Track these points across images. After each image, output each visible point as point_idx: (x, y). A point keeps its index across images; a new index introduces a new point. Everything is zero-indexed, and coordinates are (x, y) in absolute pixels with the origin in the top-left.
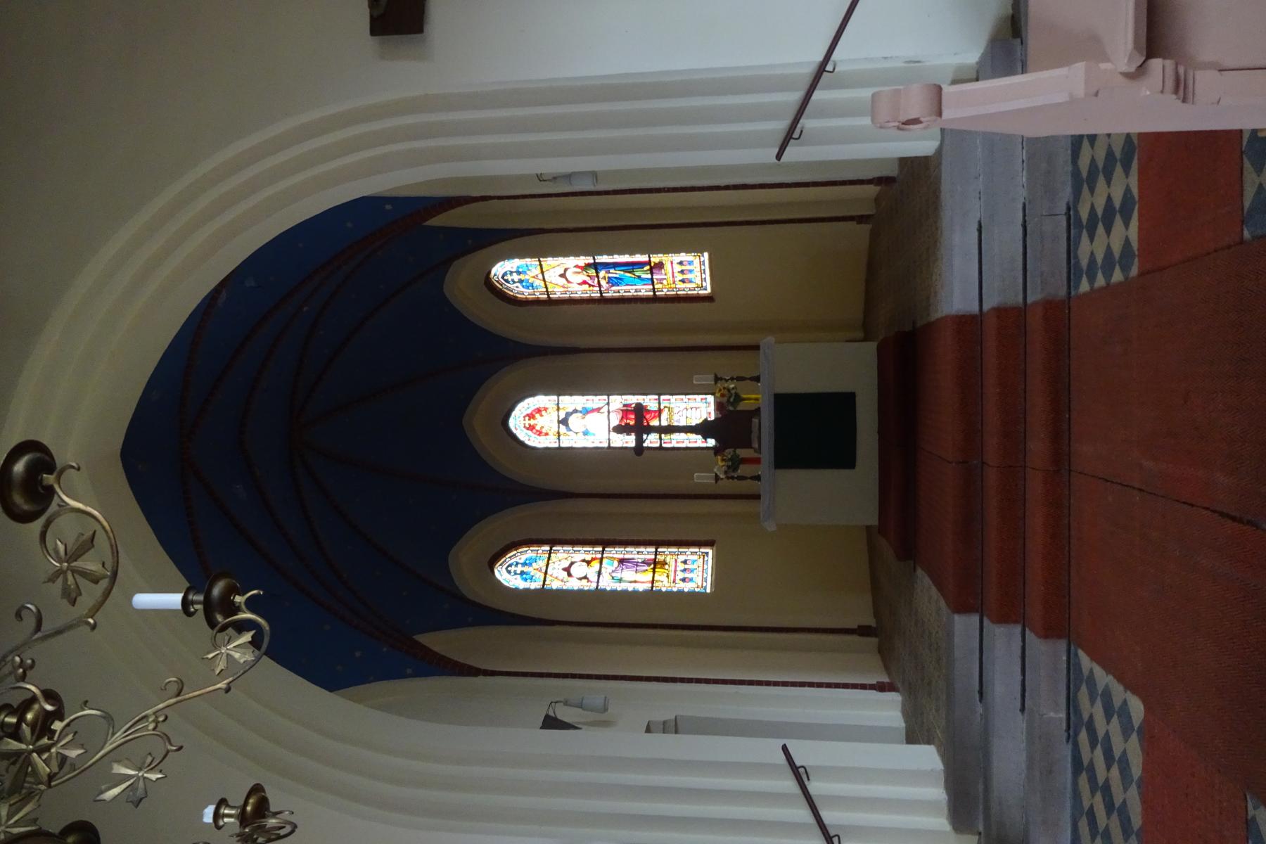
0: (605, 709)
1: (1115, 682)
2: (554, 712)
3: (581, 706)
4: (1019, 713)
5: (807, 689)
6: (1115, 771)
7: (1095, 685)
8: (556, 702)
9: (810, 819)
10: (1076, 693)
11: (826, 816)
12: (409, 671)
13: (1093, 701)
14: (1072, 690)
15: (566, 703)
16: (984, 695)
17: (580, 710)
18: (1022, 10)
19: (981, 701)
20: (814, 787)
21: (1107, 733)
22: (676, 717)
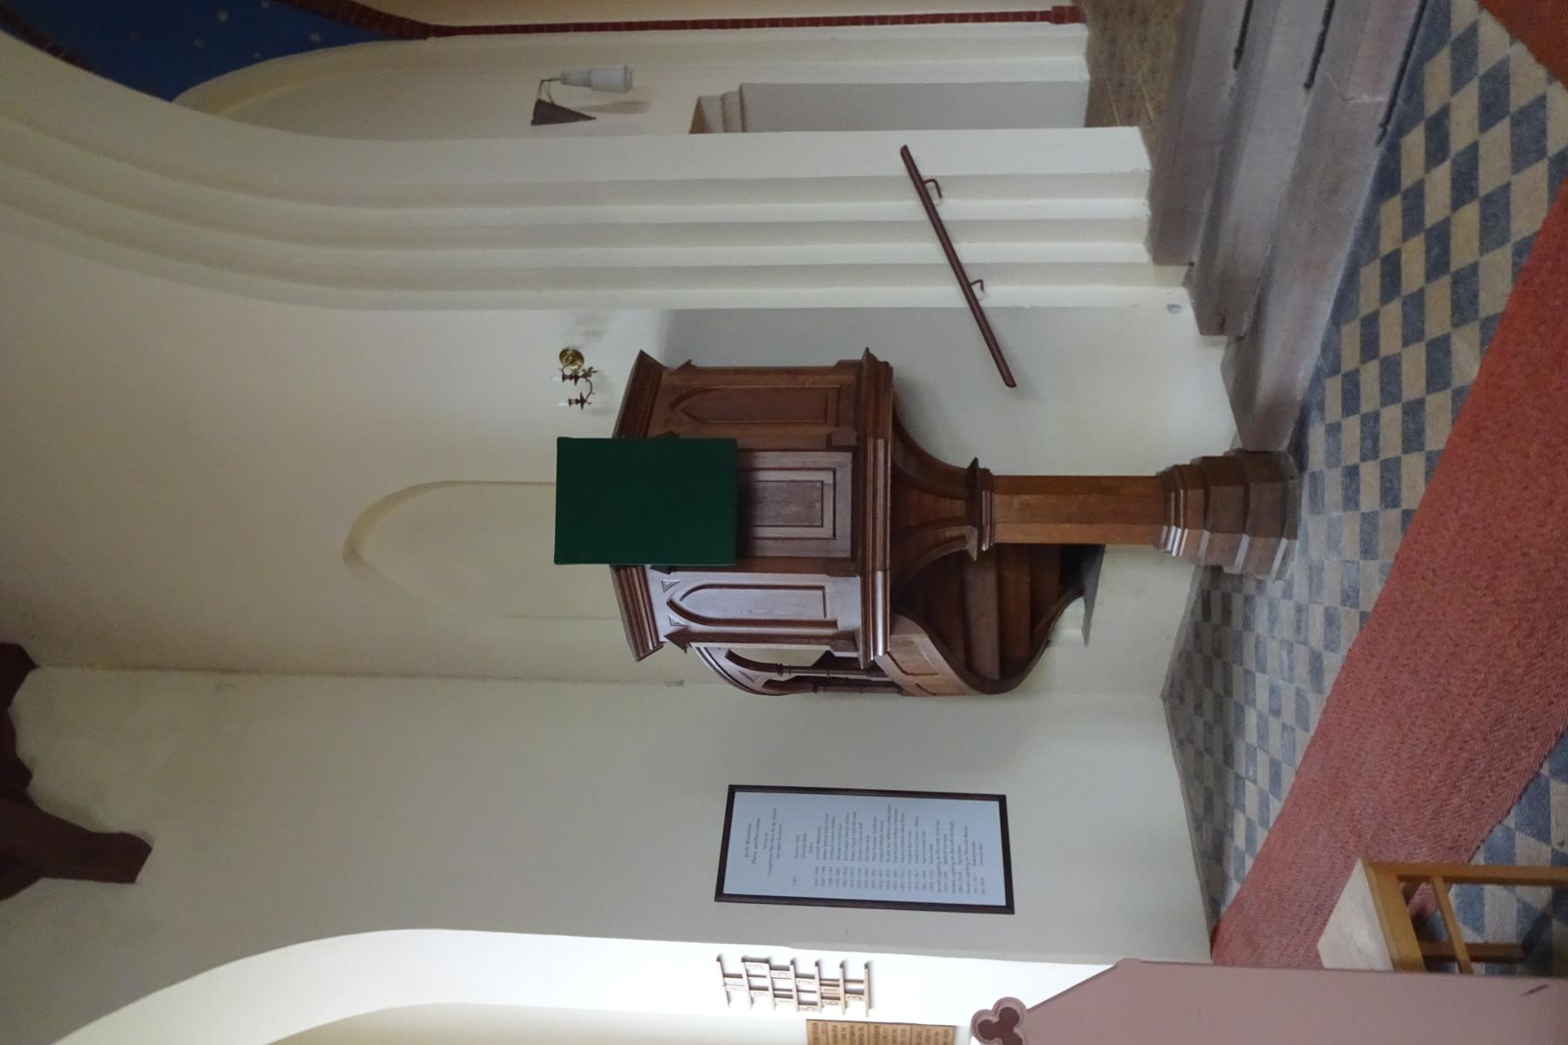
0: (627, 86)
1: (1530, 60)
2: (550, 97)
3: (587, 83)
4: (1301, 88)
5: (943, 26)
6: (1470, 214)
7: (1476, 54)
8: (550, 80)
9: (939, 257)
10: (1421, 63)
11: (964, 250)
12: (315, 37)
13: (1458, 82)
14: (1413, 56)
15: (565, 80)
16: (1244, 57)
17: (589, 90)
18: (615, 575)
19: (1236, 66)
20: (948, 209)
21: (1474, 147)
22: (741, 89)
